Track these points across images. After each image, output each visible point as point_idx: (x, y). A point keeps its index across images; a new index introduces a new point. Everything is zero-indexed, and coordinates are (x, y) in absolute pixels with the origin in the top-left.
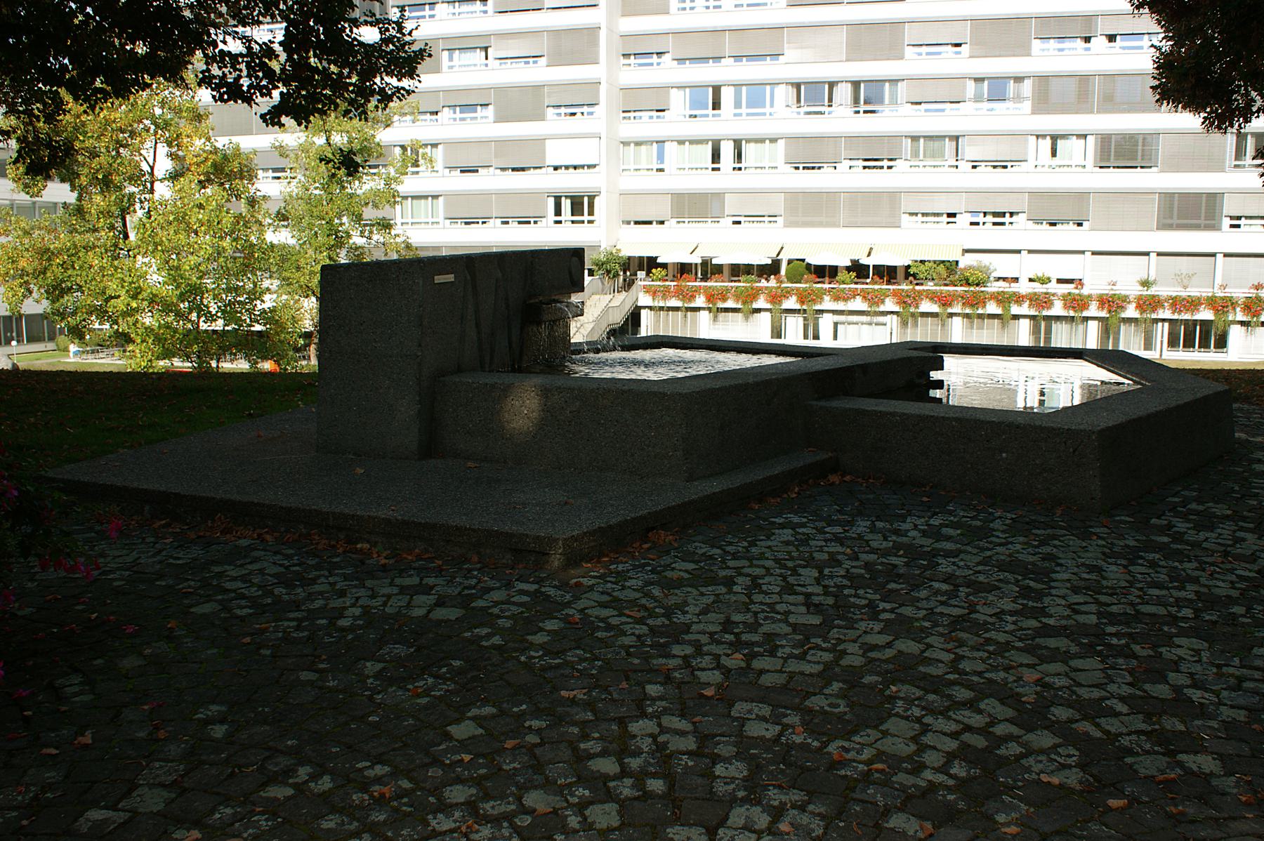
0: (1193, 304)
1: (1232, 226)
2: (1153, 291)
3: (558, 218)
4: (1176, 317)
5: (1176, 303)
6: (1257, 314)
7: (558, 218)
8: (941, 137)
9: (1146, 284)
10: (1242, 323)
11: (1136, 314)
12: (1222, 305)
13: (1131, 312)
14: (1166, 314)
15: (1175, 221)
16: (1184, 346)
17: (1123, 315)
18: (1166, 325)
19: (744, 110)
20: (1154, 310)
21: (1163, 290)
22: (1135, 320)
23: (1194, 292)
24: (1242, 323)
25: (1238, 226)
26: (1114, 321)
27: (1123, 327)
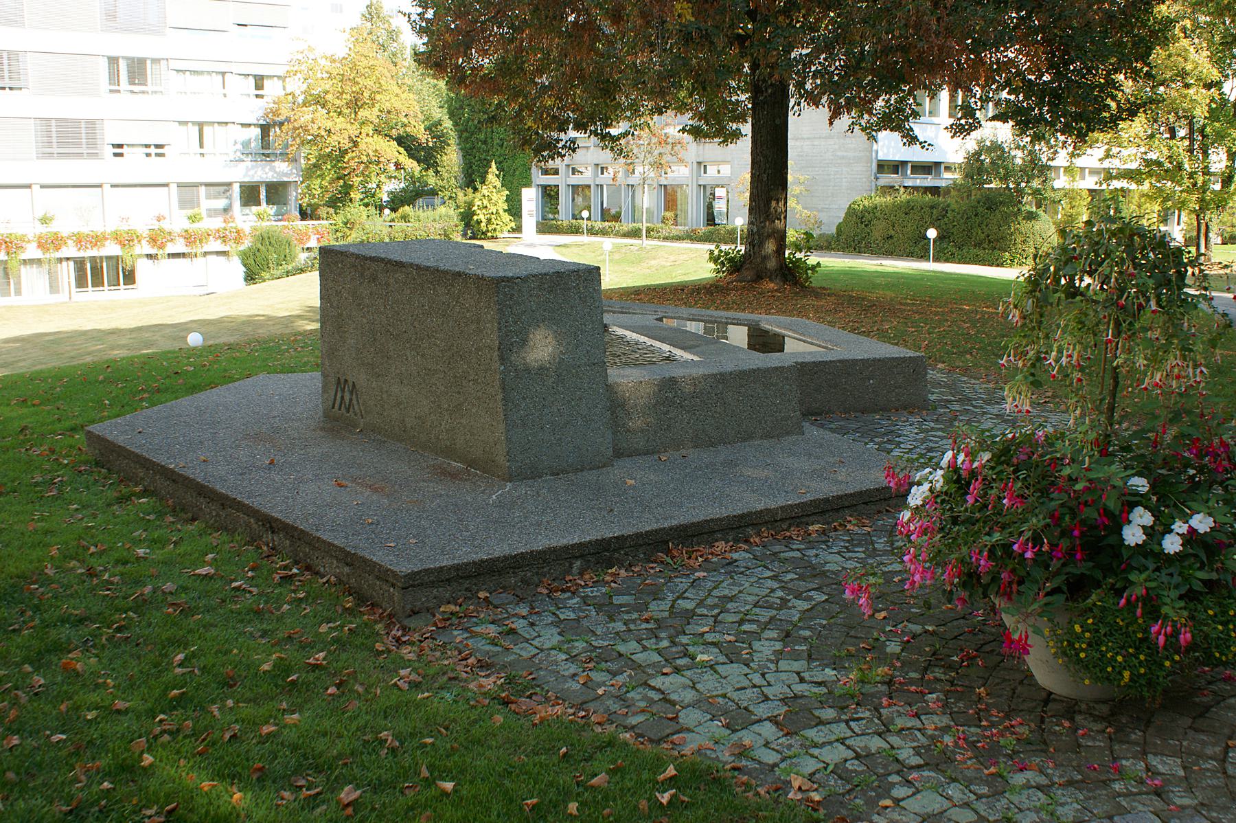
0: (97, 240)
1: (116, 155)
2: (54, 227)
3: (202, 151)
4: (81, 254)
5: (79, 240)
6: (162, 247)
7: (202, 151)
8: (196, 185)
9: (45, 220)
10: (150, 256)
11: (38, 254)
12: (125, 240)
13: (32, 252)
14: (70, 251)
15: (55, 150)
16: (96, 147)
17: (23, 256)
18: (71, 264)
19: (55, 150)
20: (57, 249)
21: (64, 226)
22: (39, 262)
23: (98, 227)
24: (150, 256)
25: (121, 155)
26: (13, 264)
27: (23, 269)
